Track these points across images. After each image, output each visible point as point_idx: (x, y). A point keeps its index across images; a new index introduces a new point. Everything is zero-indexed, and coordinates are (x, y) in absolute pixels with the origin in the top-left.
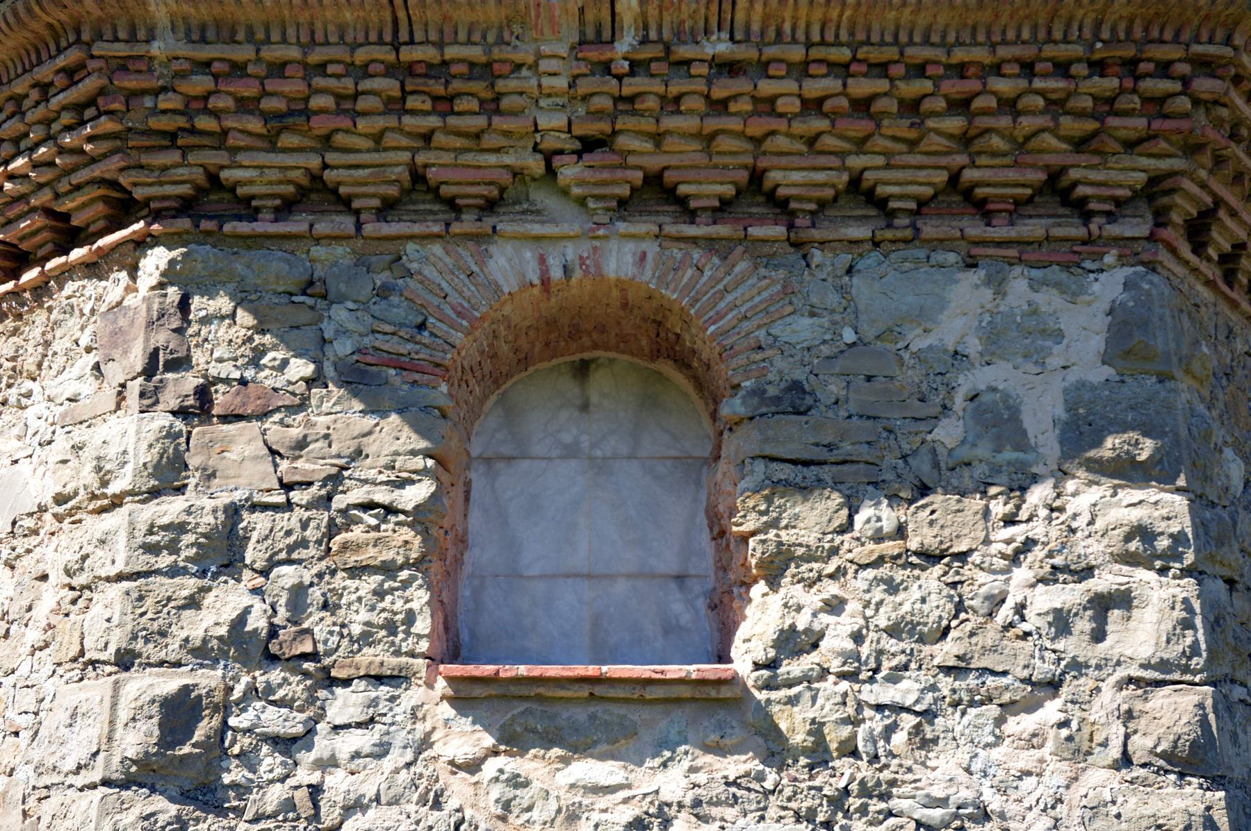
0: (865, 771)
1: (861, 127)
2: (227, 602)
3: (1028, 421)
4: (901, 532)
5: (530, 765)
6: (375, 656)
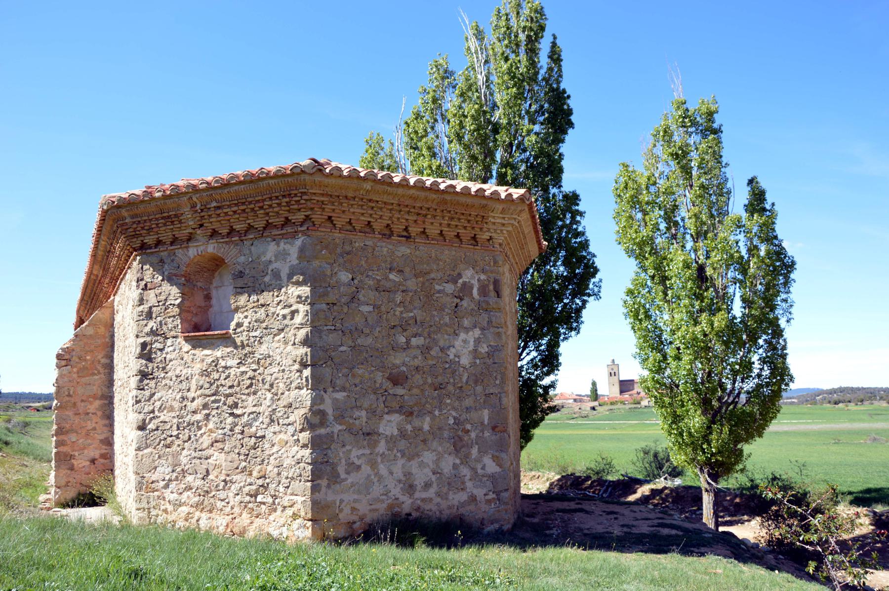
2: (152, 324)
3: (282, 275)
4: (258, 300)
6: (173, 333)
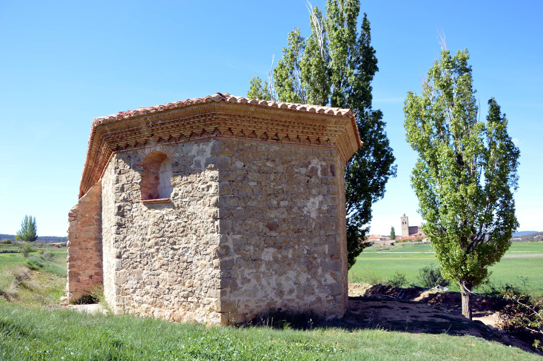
0: (183, 209)
1: (179, 128)
2: (124, 195)
4: (187, 180)
5: (151, 211)
6: (137, 200)
